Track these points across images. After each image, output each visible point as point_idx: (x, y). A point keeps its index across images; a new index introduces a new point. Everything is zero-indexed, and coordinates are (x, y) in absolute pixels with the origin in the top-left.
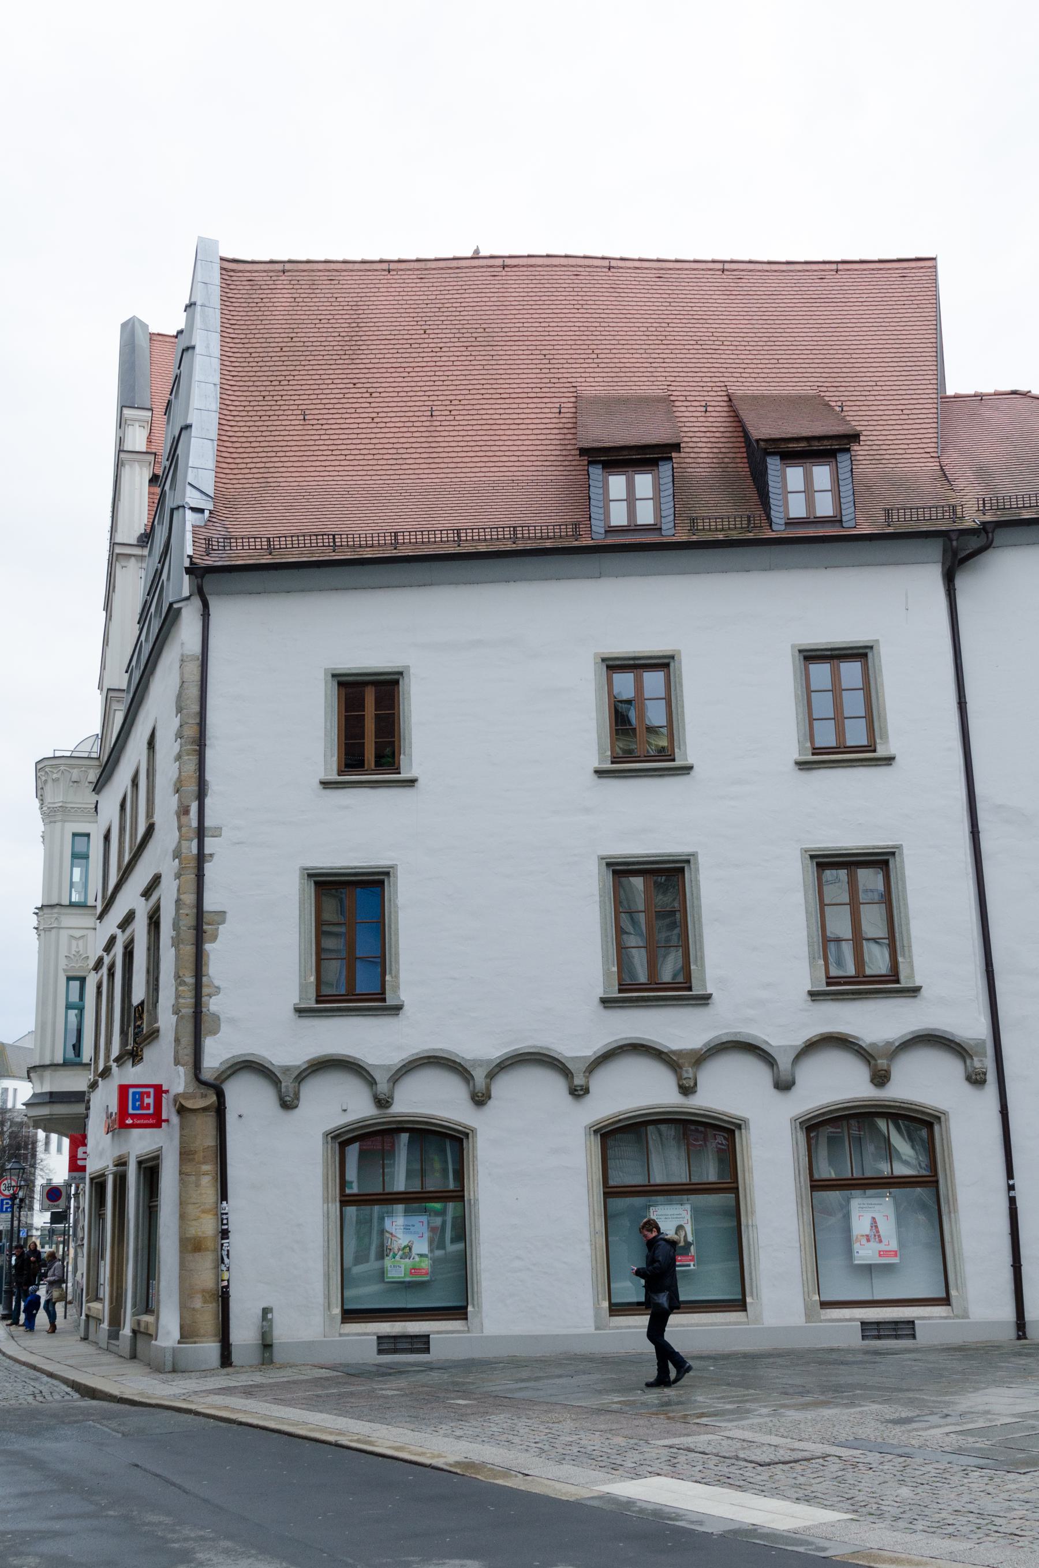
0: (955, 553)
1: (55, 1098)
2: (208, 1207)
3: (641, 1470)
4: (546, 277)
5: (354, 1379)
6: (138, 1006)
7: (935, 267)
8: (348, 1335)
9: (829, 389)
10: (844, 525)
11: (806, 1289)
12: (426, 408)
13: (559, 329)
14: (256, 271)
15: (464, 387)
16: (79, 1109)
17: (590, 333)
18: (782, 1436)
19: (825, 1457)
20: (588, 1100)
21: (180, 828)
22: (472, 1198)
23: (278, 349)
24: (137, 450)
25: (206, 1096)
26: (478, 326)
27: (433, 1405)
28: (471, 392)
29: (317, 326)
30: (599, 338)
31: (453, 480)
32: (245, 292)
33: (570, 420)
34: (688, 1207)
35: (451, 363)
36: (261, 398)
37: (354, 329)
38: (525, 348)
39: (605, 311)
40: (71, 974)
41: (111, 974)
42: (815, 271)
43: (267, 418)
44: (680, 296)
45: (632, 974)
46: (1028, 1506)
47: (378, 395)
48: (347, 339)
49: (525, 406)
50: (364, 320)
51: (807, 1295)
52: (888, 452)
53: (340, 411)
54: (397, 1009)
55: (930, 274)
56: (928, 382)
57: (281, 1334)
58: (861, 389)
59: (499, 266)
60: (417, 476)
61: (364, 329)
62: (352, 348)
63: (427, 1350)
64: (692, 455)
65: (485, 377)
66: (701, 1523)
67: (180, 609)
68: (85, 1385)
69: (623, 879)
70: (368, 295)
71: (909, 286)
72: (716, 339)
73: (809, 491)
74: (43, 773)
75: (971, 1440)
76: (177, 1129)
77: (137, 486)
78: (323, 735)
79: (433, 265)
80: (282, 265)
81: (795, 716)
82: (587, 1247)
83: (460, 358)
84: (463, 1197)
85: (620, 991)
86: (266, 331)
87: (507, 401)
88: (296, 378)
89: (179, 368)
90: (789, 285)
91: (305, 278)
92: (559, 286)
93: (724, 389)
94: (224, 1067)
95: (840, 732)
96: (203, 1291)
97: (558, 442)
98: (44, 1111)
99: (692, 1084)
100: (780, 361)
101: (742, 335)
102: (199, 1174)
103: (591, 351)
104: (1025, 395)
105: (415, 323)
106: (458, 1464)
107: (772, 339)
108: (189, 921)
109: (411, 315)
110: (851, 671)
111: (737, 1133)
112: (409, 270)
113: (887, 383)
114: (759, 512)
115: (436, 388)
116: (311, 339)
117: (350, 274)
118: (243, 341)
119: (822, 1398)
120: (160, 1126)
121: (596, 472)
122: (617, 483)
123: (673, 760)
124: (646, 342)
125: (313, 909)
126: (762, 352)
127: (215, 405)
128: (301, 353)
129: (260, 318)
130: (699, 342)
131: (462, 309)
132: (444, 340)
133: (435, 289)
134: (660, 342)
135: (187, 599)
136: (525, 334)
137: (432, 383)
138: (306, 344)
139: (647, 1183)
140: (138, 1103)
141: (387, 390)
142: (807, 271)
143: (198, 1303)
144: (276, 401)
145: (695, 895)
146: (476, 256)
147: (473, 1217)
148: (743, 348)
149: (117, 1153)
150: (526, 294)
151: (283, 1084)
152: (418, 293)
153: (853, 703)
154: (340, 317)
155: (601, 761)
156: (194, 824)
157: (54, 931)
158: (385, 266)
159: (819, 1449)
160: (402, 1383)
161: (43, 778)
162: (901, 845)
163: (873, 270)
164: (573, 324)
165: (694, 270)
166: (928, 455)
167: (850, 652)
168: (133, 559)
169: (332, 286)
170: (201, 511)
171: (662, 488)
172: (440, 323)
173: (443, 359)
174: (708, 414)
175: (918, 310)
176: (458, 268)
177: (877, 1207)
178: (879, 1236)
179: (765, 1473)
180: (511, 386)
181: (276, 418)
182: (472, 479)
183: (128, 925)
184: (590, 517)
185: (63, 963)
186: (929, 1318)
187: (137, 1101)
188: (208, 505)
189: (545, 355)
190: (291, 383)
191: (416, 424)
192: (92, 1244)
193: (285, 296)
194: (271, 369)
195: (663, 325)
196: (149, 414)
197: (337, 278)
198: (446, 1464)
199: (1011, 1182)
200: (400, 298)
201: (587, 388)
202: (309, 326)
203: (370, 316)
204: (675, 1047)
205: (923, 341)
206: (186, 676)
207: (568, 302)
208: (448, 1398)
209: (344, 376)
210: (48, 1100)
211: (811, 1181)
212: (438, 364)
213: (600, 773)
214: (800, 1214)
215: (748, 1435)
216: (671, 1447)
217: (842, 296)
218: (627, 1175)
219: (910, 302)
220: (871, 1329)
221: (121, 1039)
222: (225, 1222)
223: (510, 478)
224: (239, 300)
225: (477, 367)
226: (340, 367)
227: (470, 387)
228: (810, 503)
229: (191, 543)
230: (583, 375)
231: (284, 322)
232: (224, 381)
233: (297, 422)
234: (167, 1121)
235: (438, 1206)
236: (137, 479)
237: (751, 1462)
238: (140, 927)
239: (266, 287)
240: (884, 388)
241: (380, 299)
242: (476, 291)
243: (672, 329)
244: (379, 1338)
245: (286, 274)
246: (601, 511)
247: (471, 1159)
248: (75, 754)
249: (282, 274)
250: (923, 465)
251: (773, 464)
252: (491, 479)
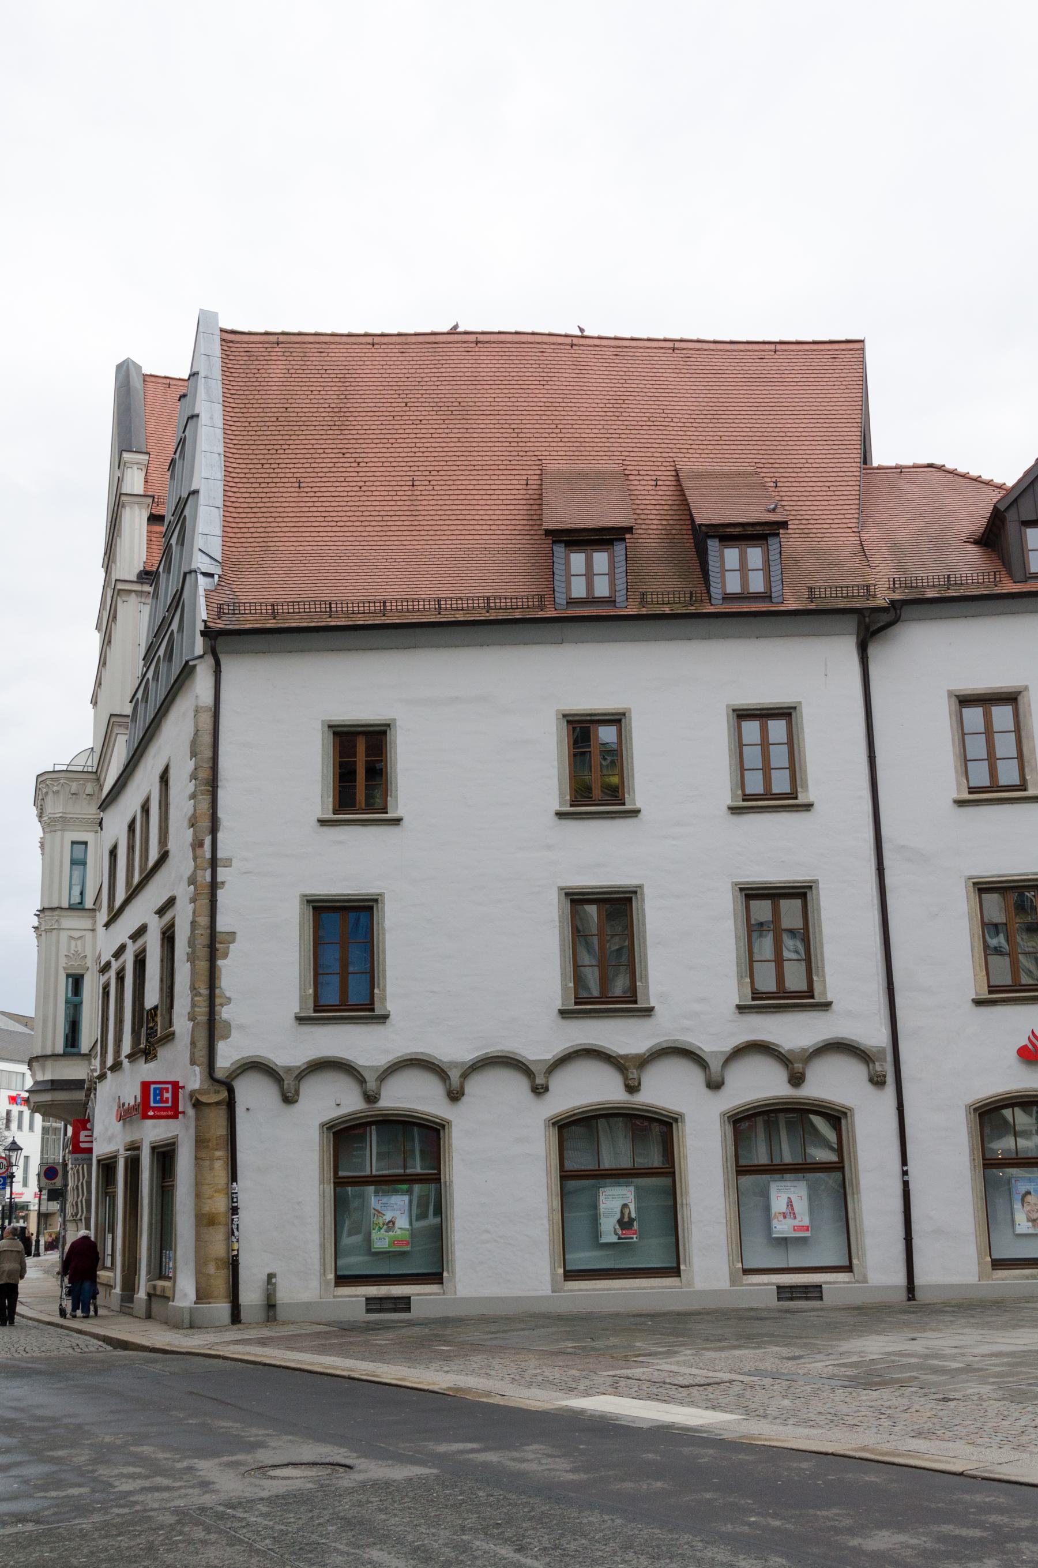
0: (867, 628)
1: (56, 1085)
2: (220, 1187)
3: (590, 1391)
4: (514, 354)
5: (348, 1333)
6: (150, 1010)
7: (863, 349)
8: (339, 1297)
9: (766, 466)
10: (773, 600)
11: (731, 1258)
12: (407, 478)
13: (526, 404)
14: (253, 343)
15: (441, 459)
16: (80, 1095)
17: (554, 409)
18: (701, 1369)
19: (731, 1382)
20: (548, 1096)
21: (195, 858)
22: (448, 1180)
23: (275, 419)
24: (136, 492)
25: (219, 1092)
26: (454, 400)
27: (422, 1350)
28: (448, 463)
29: (309, 397)
30: (562, 413)
31: (433, 547)
32: (243, 362)
33: (536, 492)
34: (632, 1188)
35: (430, 436)
36: (260, 466)
37: (342, 401)
38: (496, 422)
39: (568, 388)
40: (69, 971)
41: (120, 978)
42: (756, 351)
43: (266, 485)
44: (635, 374)
45: (588, 989)
46: (871, 1409)
47: (364, 464)
48: (336, 410)
49: (496, 477)
50: (352, 392)
51: (731, 1263)
52: (815, 526)
53: (331, 480)
54: (384, 1018)
55: (858, 356)
56: (852, 460)
57: (284, 1295)
58: (794, 466)
59: (472, 342)
60: (400, 543)
61: (351, 401)
62: (341, 419)
63: (408, 1310)
64: (643, 527)
65: (460, 449)
66: (634, 1422)
67: (194, 666)
68: (117, 1339)
69: (579, 907)
70: (354, 367)
71: (839, 367)
72: (666, 416)
73: (744, 569)
74: (44, 786)
75: (843, 1369)
76: (193, 1119)
77: (137, 526)
78: (320, 779)
79: (413, 339)
80: (277, 336)
81: (728, 766)
82: (545, 1222)
83: (438, 431)
84: (440, 1179)
85: (576, 1003)
86: (263, 401)
87: (480, 473)
88: (291, 447)
89: (184, 432)
90: (732, 364)
91: (298, 350)
92: (526, 362)
93: (672, 464)
94: (234, 1067)
95: (767, 781)
96: (216, 1259)
97: (525, 512)
98: (46, 1097)
99: (636, 1084)
100: (723, 438)
101: (689, 412)
102: (212, 1160)
103: (554, 426)
104: (940, 468)
105: (397, 396)
106: (449, 1389)
107: (716, 417)
108: (202, 940)
109: (394, 388)
110: (777, 729)
111: (674, 1126)
112: (391, 344)
113: (817, 461)
114: (700, 588)
115: (416, 459)
116: (304, 410)
117: (338, 346)
118: (242, 411)
119: (736, 1343)
120: (177, 1118)
121: (560, 550)
122: (578, 560)
123: (624, 804)
124: (604, 418)
125: (312, 930)
126: (707, 429)
127: (219, 474)
128: (295, 423)
129: (258, 388)
130: (651, 419)
131: (439, 383)
132: (423, 413)
133: (414, 363)
134: (616, 418)
135: (201, 657)
136: (496, 408)
137: (412, 454)
138: (300, 414)
139: (597, 1168)
140: (158, 1098)
141: (373, 460)
142: (749, 351)
143: (211, 1269)
144: (274, 469)
145: (641, 922)
146: (453, 331)
147: (448, 1197)
148: (690, 425)
149: (129, 1139)
150: (496, 370)
151: (286, 1082)
152: (399, 367)
153: (779, 756)
154: (329, 388)
155: (561, 805)
156: (208, 855)
157: (55, 932)
158: (369, 340)
159: (727, 1376)
160: (391, 1335)
161: (44, 790)
162: (818, 880)
163: (807, 351)
164: (538, 400)
165: (648, 348)
166: (850, 530)
167: (777, 711)
168: (133, 595)
169: (322, 359)
170: (211, 575)
171: (617, 565)
172: (420, 396)
173: (423, 431)
174: (658, 488)
175: (846, 391)
176: (435, 343)
177: (793, 1189)
178: (794, 1214)
179: (684, 1392)
180: (484, 458)
181: (274, 485)
182: (449, 546)
183: (140, 936)
184: (554, 591)
185: (63, 962)
186: (834, 1283)
187: (158, 1095)
188: (217, 570)
189: (514, 429)
190: (286, 452)
191: (399, 493)
192: (99, 1219)
193: (280, 367)
194: (269, 438)
195: (619, 402)
196: (146, 457)
197: (326, 350)
198: (440, 1389)
199: (905, 1168)
200: (384, 371)
201: (551, 462)
202: (301, 397)
203: (357, 388)
204: (622, 1051)
205: (850, 421)
206: (200, 725)
207: (534, 378)
208: (432, 1346)
209: (335, 446)
210: (49, 1087)
211: (737, 1166)
212: (418, 436)
213: (560, 815)
214: (727, 1195)
215: (674, 1368)
216: (614, 1376)
217: (779, 376)
218: (580, 1161)
219: (839, 383)
220: (785, 1292)
221: (133, 1038)
222: (235, 1200)
223: (483, 546)
224: (238, 371)
225: (453, 440)
226: (331, 437)
227: (447, 459)
228: (744, 581)
229: (205, 607)
230: (548, 449)
231: (279, 392)
232: (227, 450)
233: (293, 490)
234: (183, 1113)
235: (405, 1187)
236: (137, 520)
237: (675, 1385)
238: (153, 943)
239: (262, 358)
240: (814, 465)
241: (365, 371)
242: (452, 366)
243: (627, 406)
244: (367, 1299)
245: (280, 346)
246: (563, 585)
247: (447, 1147)
248: (71, 768)
249: (276, 345)
250: (845, 539)
251: (713, 545)
252: (466, 546)
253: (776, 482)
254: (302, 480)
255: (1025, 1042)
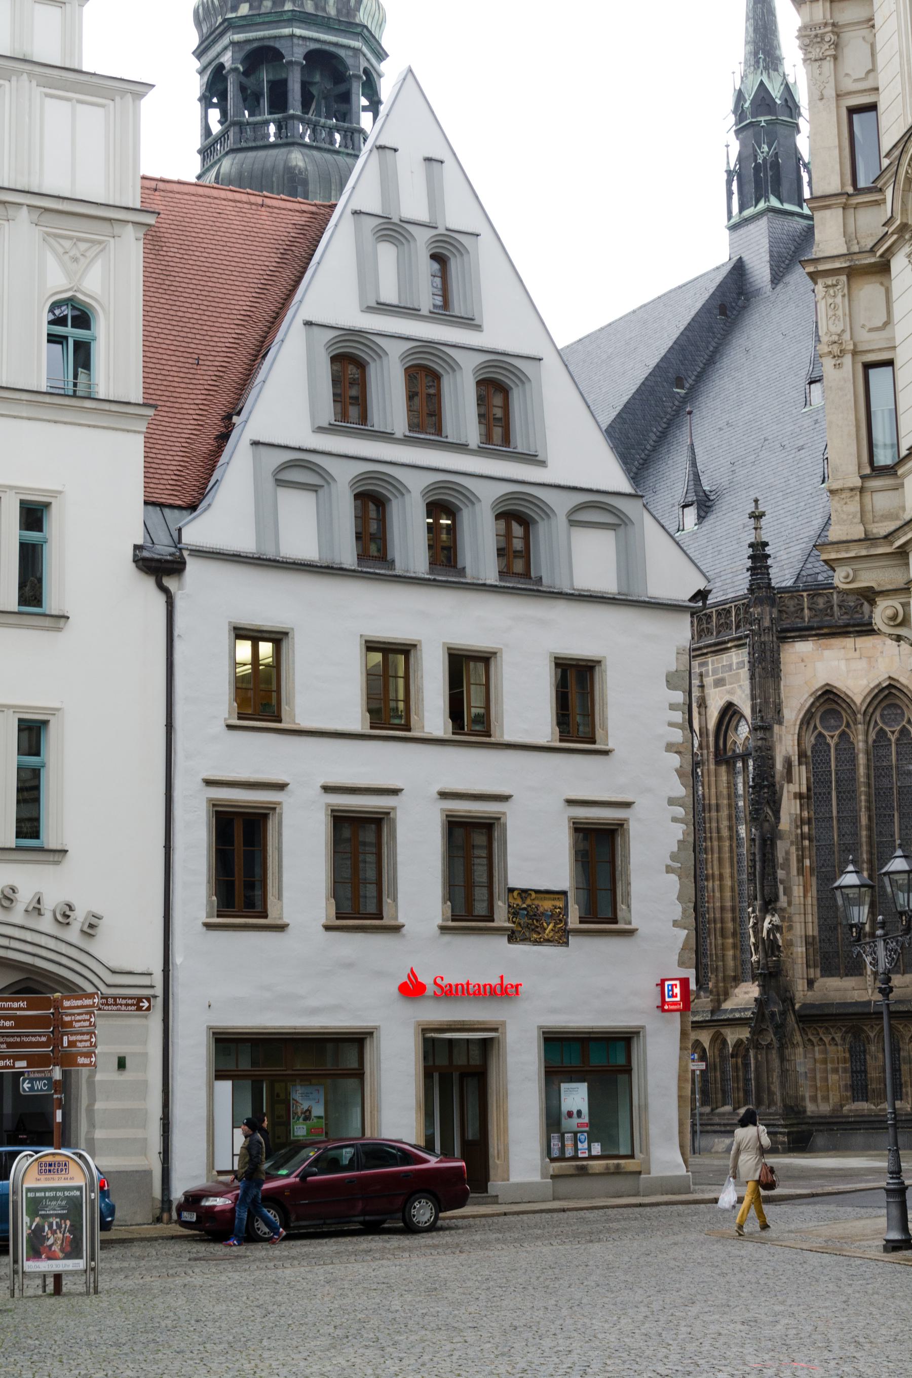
253: (198, 364)
254: (202, 357)
255: (406, 979)
